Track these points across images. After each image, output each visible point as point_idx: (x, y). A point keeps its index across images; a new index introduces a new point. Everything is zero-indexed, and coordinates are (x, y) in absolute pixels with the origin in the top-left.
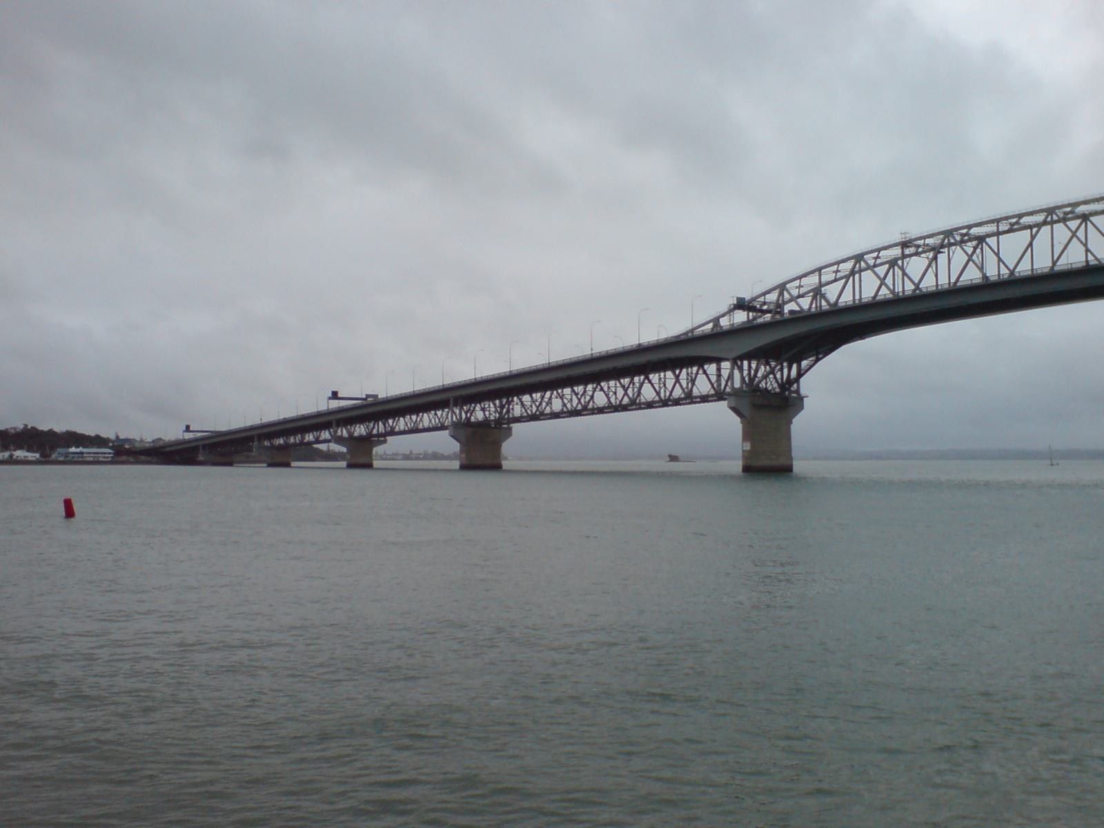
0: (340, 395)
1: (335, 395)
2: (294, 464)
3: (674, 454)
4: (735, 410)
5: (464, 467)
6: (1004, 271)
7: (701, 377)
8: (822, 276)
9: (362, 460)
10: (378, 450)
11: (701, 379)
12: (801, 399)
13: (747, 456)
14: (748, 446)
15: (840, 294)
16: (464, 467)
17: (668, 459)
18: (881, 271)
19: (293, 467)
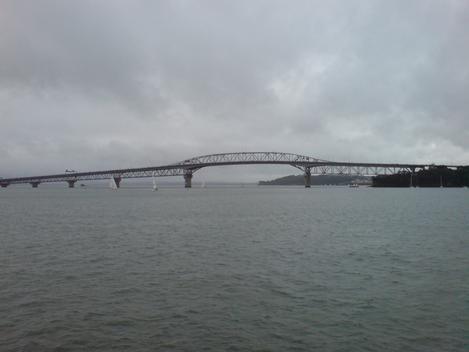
0: (68, 171)
1: (67, 171)
2: (311, 186)
3: (82, 184)
4: (185, 178)
5: (70, 187)
6: (214, 162)
7: (102, 176)
8: (242, 154)
9: (72, 186)
10: (75, 184)
11: (93, 177)
12: (192, 176)
13: (186, 185)
14: (186, 183)
15: (201, 160)
16: (70, 187)
17: (81, 185)
18: (195, 160)
19: (193, 188)
